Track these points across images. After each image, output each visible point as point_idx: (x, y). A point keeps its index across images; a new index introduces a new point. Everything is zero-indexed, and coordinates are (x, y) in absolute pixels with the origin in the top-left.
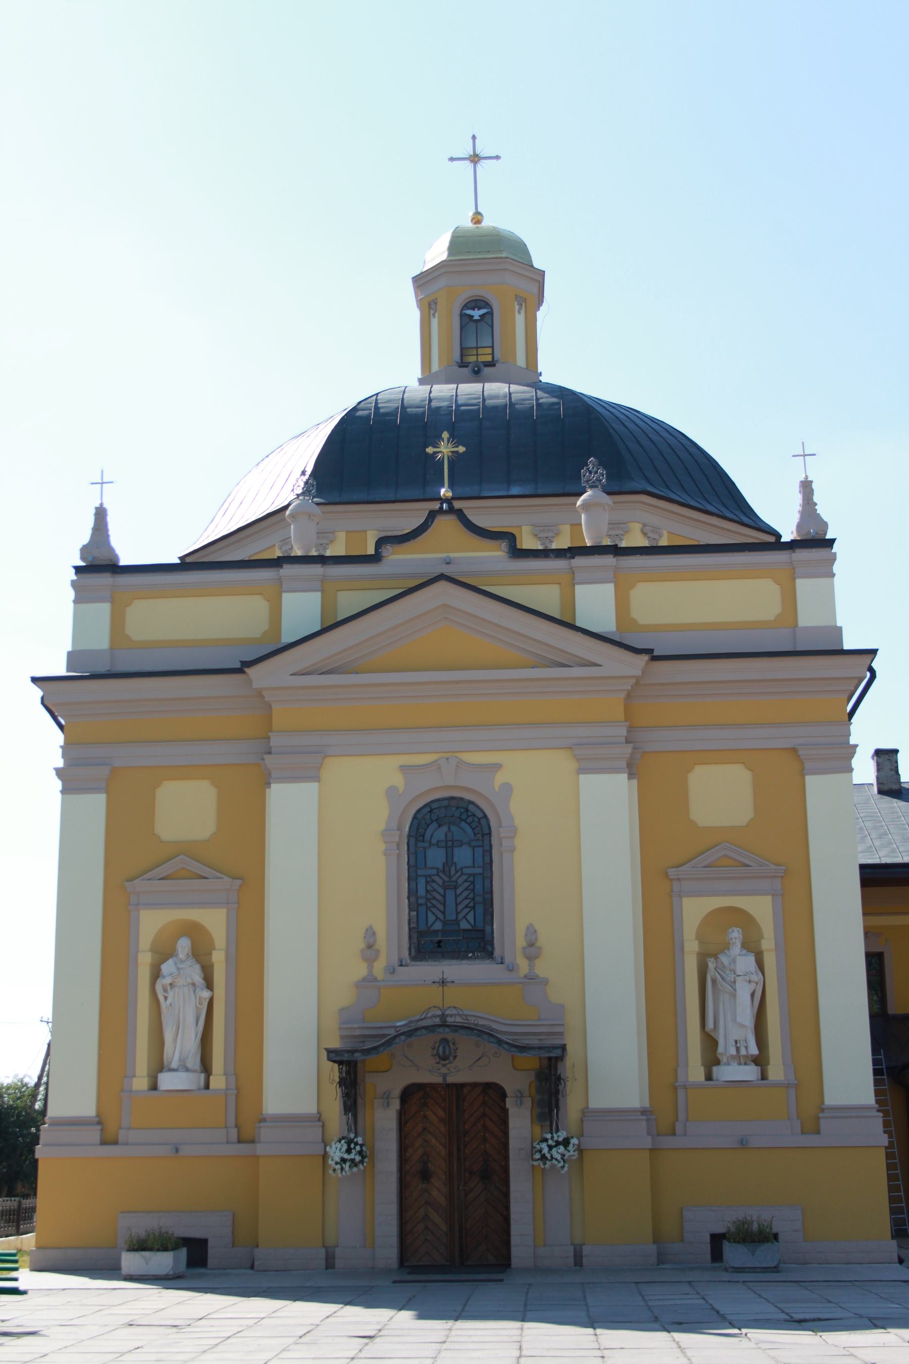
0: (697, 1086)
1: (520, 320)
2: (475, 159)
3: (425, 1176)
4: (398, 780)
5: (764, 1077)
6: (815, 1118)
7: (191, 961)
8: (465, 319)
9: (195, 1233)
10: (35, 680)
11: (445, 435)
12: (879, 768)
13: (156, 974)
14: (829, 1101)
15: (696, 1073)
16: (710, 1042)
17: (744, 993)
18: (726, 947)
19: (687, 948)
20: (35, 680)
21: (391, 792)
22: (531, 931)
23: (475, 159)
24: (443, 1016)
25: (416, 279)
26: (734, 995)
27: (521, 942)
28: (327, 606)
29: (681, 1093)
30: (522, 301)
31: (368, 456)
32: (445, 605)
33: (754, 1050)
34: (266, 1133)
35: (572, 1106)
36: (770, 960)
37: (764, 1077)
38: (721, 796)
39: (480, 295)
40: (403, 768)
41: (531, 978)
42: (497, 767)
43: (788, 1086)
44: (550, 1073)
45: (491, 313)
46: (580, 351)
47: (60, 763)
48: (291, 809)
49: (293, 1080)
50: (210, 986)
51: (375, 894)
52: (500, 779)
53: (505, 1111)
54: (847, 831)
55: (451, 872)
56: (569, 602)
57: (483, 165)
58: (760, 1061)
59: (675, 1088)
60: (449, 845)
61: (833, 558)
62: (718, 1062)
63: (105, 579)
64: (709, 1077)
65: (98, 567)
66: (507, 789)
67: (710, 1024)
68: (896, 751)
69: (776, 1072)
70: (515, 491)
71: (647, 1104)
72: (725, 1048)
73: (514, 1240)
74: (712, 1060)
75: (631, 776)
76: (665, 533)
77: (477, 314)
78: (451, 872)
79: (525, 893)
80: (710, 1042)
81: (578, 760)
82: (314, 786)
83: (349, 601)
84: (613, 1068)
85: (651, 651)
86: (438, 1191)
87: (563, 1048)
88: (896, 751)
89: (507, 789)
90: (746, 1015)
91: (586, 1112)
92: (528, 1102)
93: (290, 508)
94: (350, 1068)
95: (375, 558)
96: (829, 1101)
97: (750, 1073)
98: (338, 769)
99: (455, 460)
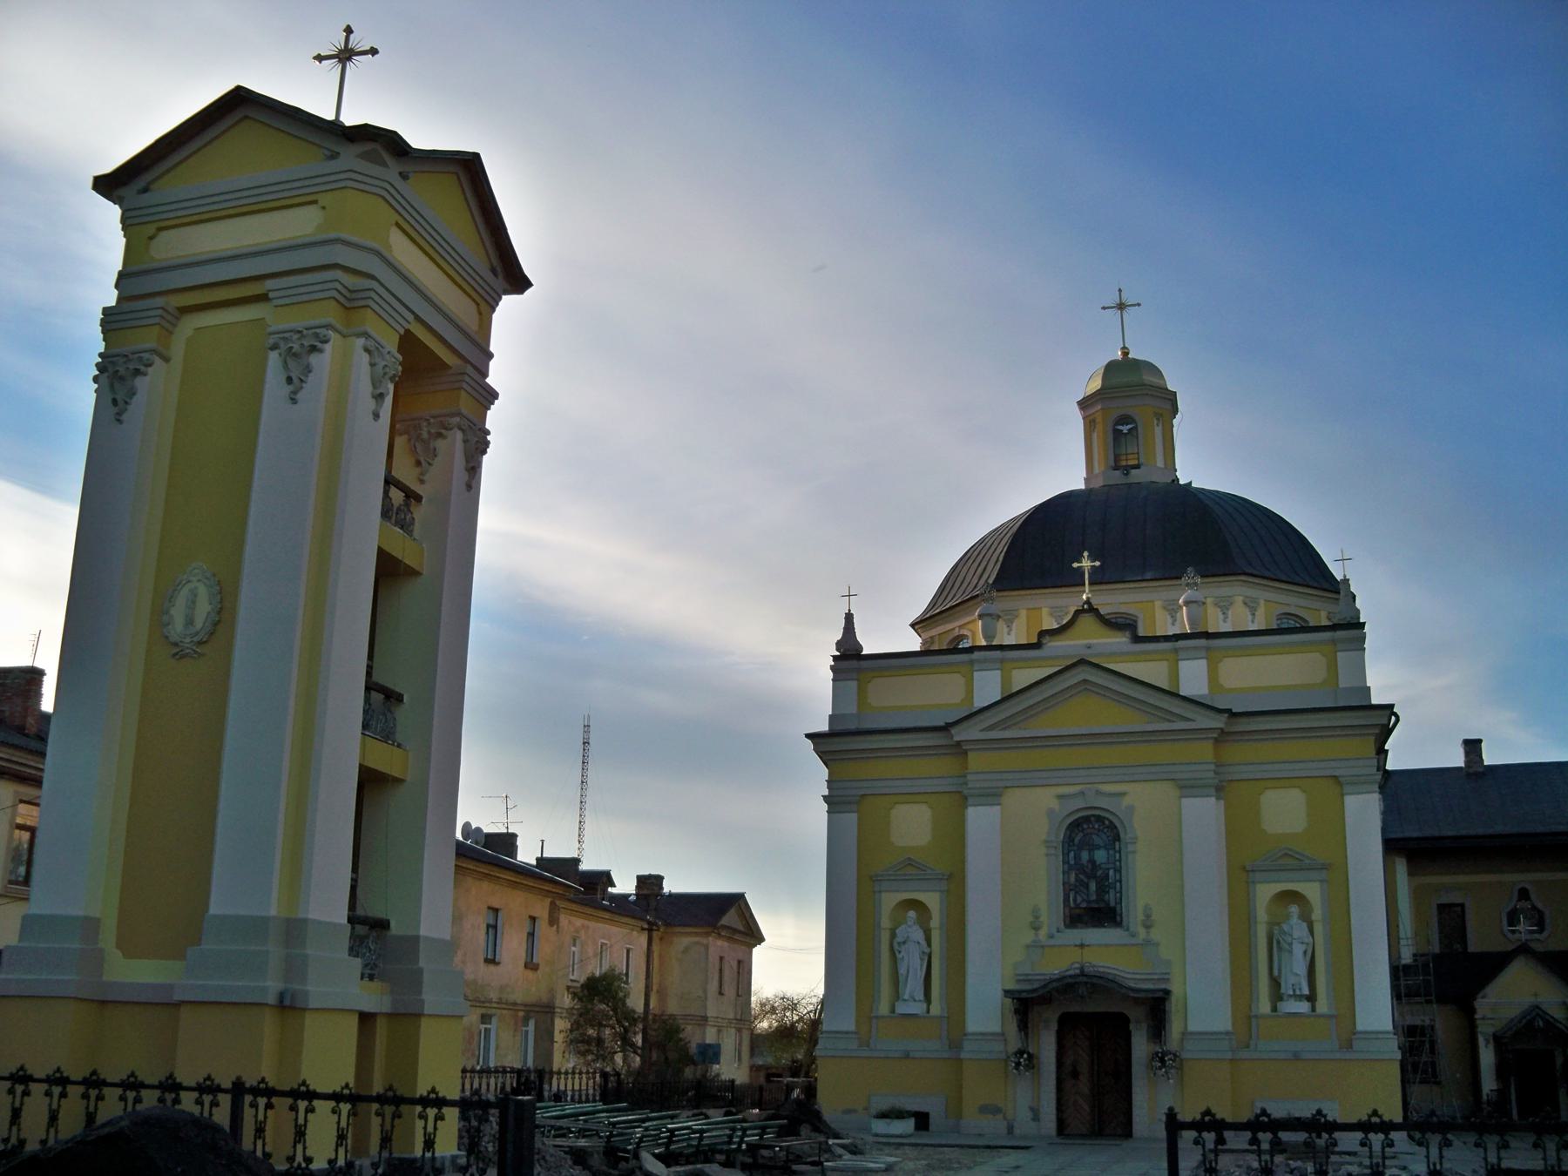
0: (1264, 1017)
1: (1158, 431)
2: (1121, 306)
3: (1075, 1074)
4: (1054, 804)
5: (1313, 1009)
6: (1349, 1038)
7: (916, 927)
8: (1117, 434)
9: (922, 1109)
10: (808, 736)
11: (1086, 554)
12: (1467, 754)
13: (893, 935)
14: (1359, 1027)
15: (1264, 1007)
16: (1275, 983)
17: (1298, 950)
18: (1288, 917)
19: (1259, 919)
20: (808, 736)
21: (1050, 812)
22: (1147, 909)
23: (1121, 306)
24: (1082, 969)
25: (1079, 403)
26: (1291, 952)
27: (1141, 917)
28: (1006, 681)
29: (1254, 1022)
30: (1159, 416)
31: (1036, 549)
32: (1085, 681)
33: (1306, 991)
34: (967, 1046)
35: (1175, 1029)
36: (1318, 928)
37: (1313, 1009)
38: (1284, 812)
39: (1128, 406)
40: (1060, 797)
41: (1147, 942)
42: (1124, 794)
43: (1331, 1016)
44: (1157, 1006)
45: (1135, 428)
46: (1201, 461)
47: (826, 792)
48: (981, 820)
49: (986, 1010)
50: (929, 945)
51: (1043, 887)
52: (1126, 801)
53: (1129, 1033)
54: (707, 1168)
55: (1092, 876)
56: (1174, 675)
57: (1129, 314)
58: (1312, 998)
59: (1250, 1017)
60: (1093, 848)
61: (1363, 638)
62: (1281, 998)
63: (854, 663)
64: (1274, 1009)
65: (849, 656)
66: (1131, 809)
67: (1276, 973)
68: (1480, 741)
69: (1323, 1006)
70: (1148, 575)
71: (1230, 1028)
72: (1286, 989)
73: (1136, 1119)
74: (1277, 996)
75: (1218, 798)
76: (1262, 602)
77: (1125, 429)
78: (1092, 876)
79: (1143, 885)
80: (1275, 983)
81: (1181, 788)
82: (995, 811)
83: (1023, 677)
84: (1204, 1005)
85: (1229, 711)
86: (1084, 1085)
87: (1167, 992)
88: (1480, 741)
89: (1131, 809)
90: (1300, 967)
91: (1185, 1034)
92: (1144, 1026)
93: (987, 724)
94: (1026, 1005)
95: (1037, 646)
96: (1359, 1027)
97: (1303, 1007)
98: (1016, 799)
99: (1094, 569)
